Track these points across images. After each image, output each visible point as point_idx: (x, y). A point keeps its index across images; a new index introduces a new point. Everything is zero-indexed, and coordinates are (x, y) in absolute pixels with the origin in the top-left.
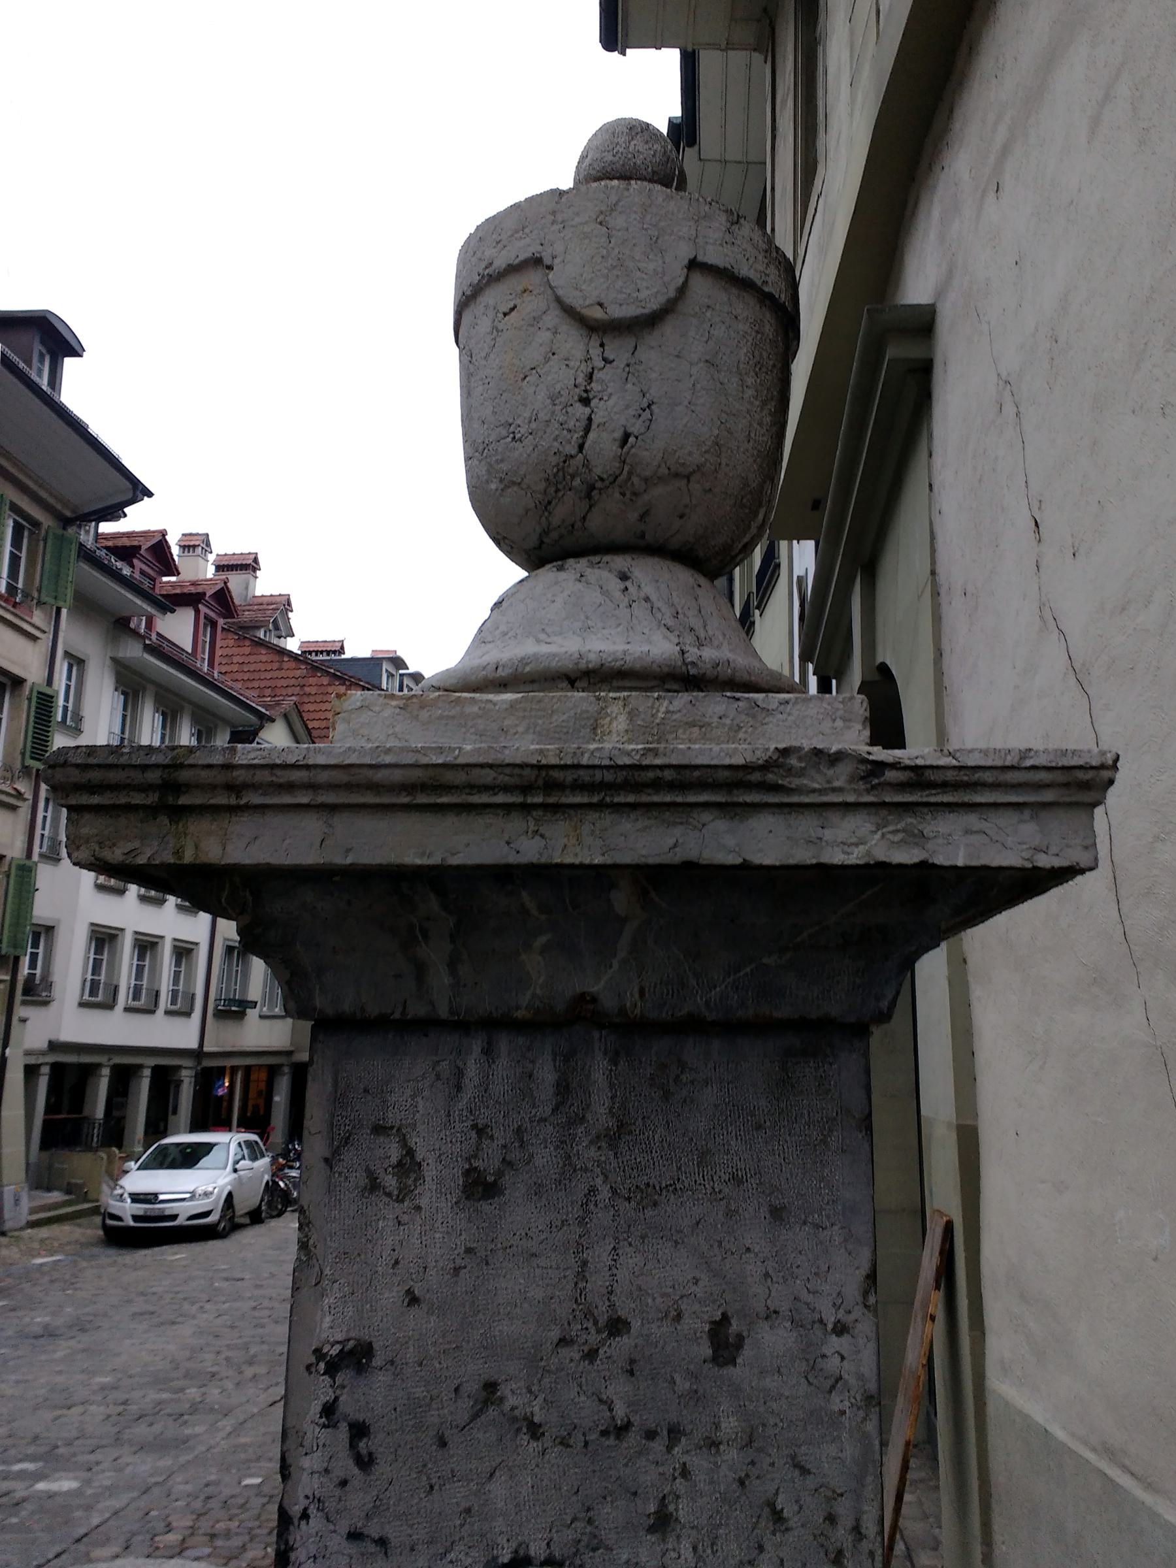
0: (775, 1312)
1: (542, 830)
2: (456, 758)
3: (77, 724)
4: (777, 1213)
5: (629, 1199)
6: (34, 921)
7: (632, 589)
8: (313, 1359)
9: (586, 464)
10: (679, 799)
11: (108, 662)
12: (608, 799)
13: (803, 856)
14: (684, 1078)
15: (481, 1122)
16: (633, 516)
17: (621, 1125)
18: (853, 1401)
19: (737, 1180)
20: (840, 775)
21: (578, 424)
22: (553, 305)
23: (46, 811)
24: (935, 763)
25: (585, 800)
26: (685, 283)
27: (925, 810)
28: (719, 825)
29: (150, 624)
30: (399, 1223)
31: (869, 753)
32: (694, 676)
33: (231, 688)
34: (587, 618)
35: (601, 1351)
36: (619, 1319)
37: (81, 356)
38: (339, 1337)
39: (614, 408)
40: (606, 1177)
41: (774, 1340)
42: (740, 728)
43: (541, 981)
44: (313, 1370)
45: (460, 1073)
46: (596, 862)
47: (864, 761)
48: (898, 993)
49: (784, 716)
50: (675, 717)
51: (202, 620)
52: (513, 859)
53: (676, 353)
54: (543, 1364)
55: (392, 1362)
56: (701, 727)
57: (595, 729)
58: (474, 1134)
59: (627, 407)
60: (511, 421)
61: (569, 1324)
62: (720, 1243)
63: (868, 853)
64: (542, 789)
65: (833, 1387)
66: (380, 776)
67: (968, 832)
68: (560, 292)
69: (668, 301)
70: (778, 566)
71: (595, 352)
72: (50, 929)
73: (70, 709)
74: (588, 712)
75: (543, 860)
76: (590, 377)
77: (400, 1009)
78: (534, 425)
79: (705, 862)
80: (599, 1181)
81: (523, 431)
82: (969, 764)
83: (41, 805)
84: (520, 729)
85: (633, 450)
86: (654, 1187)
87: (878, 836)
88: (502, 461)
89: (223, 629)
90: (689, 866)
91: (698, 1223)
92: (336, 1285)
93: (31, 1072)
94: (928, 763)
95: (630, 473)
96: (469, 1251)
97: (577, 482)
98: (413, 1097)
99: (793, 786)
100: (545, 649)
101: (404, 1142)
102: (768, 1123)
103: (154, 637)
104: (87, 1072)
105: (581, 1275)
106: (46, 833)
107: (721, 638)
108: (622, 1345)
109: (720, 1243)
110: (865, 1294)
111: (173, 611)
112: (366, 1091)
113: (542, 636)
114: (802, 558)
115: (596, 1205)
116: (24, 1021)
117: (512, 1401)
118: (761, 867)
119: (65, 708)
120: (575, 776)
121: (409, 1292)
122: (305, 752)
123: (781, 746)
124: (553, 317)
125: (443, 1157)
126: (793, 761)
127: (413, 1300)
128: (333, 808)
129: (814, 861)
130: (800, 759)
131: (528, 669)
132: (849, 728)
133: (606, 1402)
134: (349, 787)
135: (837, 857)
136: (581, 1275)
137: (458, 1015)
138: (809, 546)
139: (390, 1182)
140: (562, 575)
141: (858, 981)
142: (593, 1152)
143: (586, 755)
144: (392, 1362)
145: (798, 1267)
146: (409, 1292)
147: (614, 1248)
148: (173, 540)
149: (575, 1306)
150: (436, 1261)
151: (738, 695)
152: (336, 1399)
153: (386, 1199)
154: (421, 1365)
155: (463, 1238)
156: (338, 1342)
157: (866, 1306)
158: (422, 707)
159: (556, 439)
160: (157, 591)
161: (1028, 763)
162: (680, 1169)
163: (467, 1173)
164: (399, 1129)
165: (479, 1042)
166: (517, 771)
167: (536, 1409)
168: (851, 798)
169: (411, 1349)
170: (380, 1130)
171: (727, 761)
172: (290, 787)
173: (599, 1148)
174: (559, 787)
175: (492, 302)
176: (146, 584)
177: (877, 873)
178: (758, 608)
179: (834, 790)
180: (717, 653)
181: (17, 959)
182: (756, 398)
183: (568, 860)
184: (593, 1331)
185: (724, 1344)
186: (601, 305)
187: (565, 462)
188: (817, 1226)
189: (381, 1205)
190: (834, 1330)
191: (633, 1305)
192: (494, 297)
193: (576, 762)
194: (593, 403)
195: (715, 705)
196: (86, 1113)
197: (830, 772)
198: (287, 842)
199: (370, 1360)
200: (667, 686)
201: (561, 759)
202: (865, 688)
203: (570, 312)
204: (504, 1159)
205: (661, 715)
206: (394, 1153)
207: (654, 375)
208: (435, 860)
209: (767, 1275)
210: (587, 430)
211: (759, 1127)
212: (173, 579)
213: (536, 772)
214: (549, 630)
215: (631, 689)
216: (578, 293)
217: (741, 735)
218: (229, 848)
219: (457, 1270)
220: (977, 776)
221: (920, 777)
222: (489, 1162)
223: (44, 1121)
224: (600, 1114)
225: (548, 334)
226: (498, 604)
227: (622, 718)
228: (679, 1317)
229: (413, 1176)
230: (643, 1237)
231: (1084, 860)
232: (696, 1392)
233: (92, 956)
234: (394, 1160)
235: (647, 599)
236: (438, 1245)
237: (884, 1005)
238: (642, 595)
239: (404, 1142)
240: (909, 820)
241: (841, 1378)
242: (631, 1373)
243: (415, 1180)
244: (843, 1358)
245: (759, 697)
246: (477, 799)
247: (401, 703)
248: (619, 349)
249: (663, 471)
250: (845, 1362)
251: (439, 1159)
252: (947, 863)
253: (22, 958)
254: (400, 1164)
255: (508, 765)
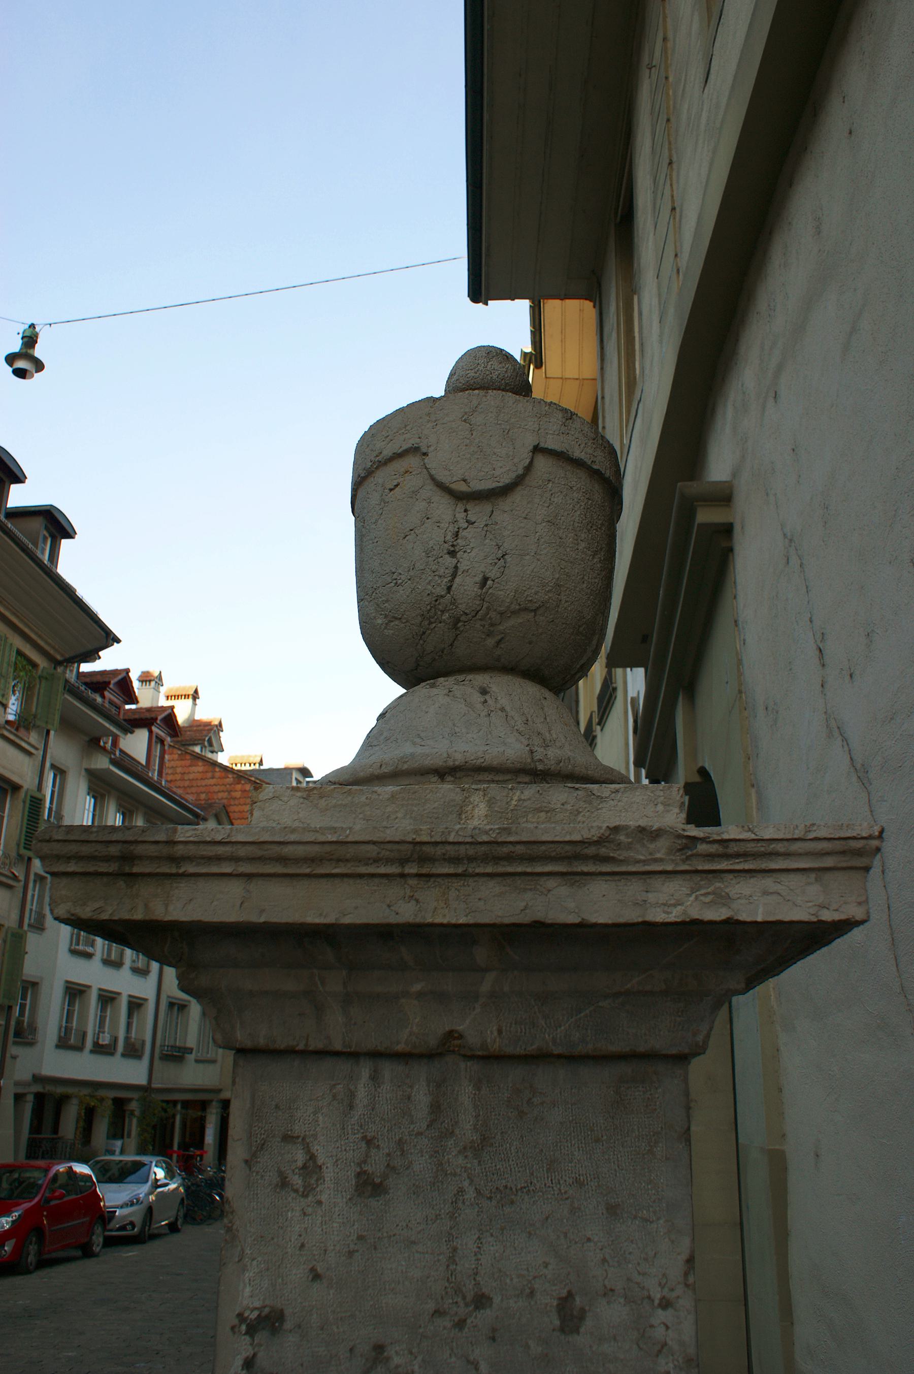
0: (612, 1290)
1: (417, 895)
2: (347, 836)
3: (58, 821)
4: (613, 1210)
5: (490, 1198)
6: (24, 978)
7: (490, 702)
8: (236, 1321)
9: (454, 602)
10: (529, 870)
11: (83, 773)
12: (470, 870)
13: (631, 915)
14: (535, 1100)
15: (369, 1135)
16: (491, 642)
17: (484, 1139)
18: (676, 1363)
19: (579, 1183)
20: (661, 848)
21: (447, 571)
22: (429, 481)
23: (34, 891)
24: (737, 837)
25: (452, 871)
26: (531, 463)
27: (731, 876)
28: (560, 891)
29: (115, 743)
30: (305, 1214)
31: (684, 830)
32: (541, 770)
33: (175, 793)
34: (454, 725)
35: (469, 1321)
36: (483, 1295)
37: (23, 482)
38: (257, 1304)
39: (476, 559)
40: (472, 1181)
41: (612, 1313)
42: (579, 813)
43: (417, 1020)
44: (236, 1330)
45: (352, 1095)
46: (461, 921)
47: (679, 836)
48: (711, 1029)
49: (615, 802)
50: (526, 804)
51: (154, 739)
52: (393, 919)
53: (524, 515)
54: (421, 1330)
55: (299, 1326)
56: (547, 812)
57: (460, 811)
58: (364, 1145)
59: (486, 557)
60: (394, 570)
61: (442, 1298)
62: (566, 1235)
63: (685, 912)
64: (417, 860)
65: (660, 1351)
66: (287, 850)
67: (766, 893)
68: (433, 472)
69: (518, 477)
70: (615, 689)
71: (461, 516)
72: (35, 985)
73: (54, 809)
74: (454, 800)
75: (418, 920)
76: (457, 535)
77: (304, 1042)
78: (411, 573)
79: (550, 922)
80: (466, 1184)
81: (403, 577)
82: (765, 837)
83: (31, 885)
84: (400, 815)
85: (490, 591)
86: (511, 1188)
87: (692, 898)
88: (387, 601)
89: (170, 746)
90: (538, 925)
91: (547, 1218)
92: (255, 1262)
93: (18, 1098)
94: (732, 837)
95: (488, 608)
96: (361, 1238)
97: (446, 616)
98: (315, 1113)
99: (621, 858)
100: (419, 750)
101: (307, 1149)
102: (605, 1137)
103: (118, 753)
104: (62, 1100)
105: (452, 1260)
106: (34, 908)
107: (564, 741)
108: (486, 1316)
109: (566, 1235)
110: (686, 1274)
111: (132, 732)
112: (277, 1107)
113: (418, 740)
114: (635, 682)
115: (464, 1203)
116: (14, 1058)
117: (396, 1360)
118: (595, 925)
119: (50, 809)
120: (443, 851)
121: (313, 1270)
122: (228, 831)
123: (612, 825)
124: (429, 490)
125: (339, 1162)
126: (622, 838)
127: (316, 1276)
128: (250, 876)
129: (640, 920)
130: (627, 835)
131: (405, 766)
132: (668, 811)
133: (472, 1363)
134: (262, 859)
135: (659, 916)
136: (452, 1260)
137: (350, 1048)
138: (640, 672)
139: (297, 1181)
140: (435, 691)
141: (678, 1019)
142: (461, 1160)
143: (453, 834)
144: (299, 1326)
145: (630, 1253)
146: (313, 1270)
147: (479, 1238)
148: (134, 676)
149: (447, 1284)
150: (334, 1246)
151: (577, 786)
152: (255, 1355)
153: (293, 1195)
154: (322, 1329)
155: (355, 1227)
156: (256, 1308)
157: (687, 1285)
158: (321, 797)
159: (429, 583)
160: (121, 717)
161: (811, 835)
162: (532, 1174)
163: (359, 1175)
164: (304, 1139)
165: (367, 1070)
166: (396, 847)
167: (416, 1367)
168: (669, 868)
169: (315, 1316)
170: (288, 1138)
171: (567, 838)
172: (219, 859)
173: (466, 1157)
174: (431, 860)
175: (380, 481)
176: (114, 711)
177: (691, 930)
178: (599, 724)
179: (656, 860)
180: (561, 751)
181: (10, 1008)
182: (589, 549)
183: (439, 920)
184: (462, 1304)
185: (570, 1316)
186: (465, 481)
187: (436, 601)
188: (647, 1220)
189: (290, 1199)
190: (660, 1305)
191: (494, 1284)
192: (383, 477)
193: (444, 840)
194: (458, 555)
195: (559, 795)
196: (61, 1134)
197: (652, 846)
198: (215, 903)
199: (282, 1323)
200: (519, 780)
201: (431, 837)
202: (689, 788)
203: (433, 478)
204: (388, 1165)
205: (514, 803)
206: (300, 1157)
207: (506, 533)
208: (330, 920)
209: (604, 1260)
210: (454, 575)
211: (597, 1140)
212: (133, 707)
213: (411, 846)
214: (422, 735)
215: (489, 782)
216: (447, 473)
217: (580, 818)
218: (171, 908)
219: (351, 1254)
220: (772, 846)
221: (727, 849)
222: (376, 1166)
223: (29, 1138)
224: (467, 1129)
225: (424, 504)
226: (382, 716)
227: (482, 805)
228: (532, 1294)
229: (315, 1177)
230: (502, 1229)
231: (857, 913)
232: (547, 1355)
233: (66, 1007)
234: (300, 1163)
235: (503, 709)
236: (335, 1233)
237: (700, 1038)
238: (499, 706)
239: (307, 1149)
240: (718, 885)
241: (665, 1344)
242: (493, 1339)
243: (317, 1180)
244: (667, 1328)
245: (595, 787)
246: (363, 870)
247: (305, 794)
248: (479, 512)
249: (515, 607)
250: (670, 1331)
251: (336, 1163)
252: (749, 919)
253: (14, 1008)
254: (305, 1167)
255: (389, 842)
